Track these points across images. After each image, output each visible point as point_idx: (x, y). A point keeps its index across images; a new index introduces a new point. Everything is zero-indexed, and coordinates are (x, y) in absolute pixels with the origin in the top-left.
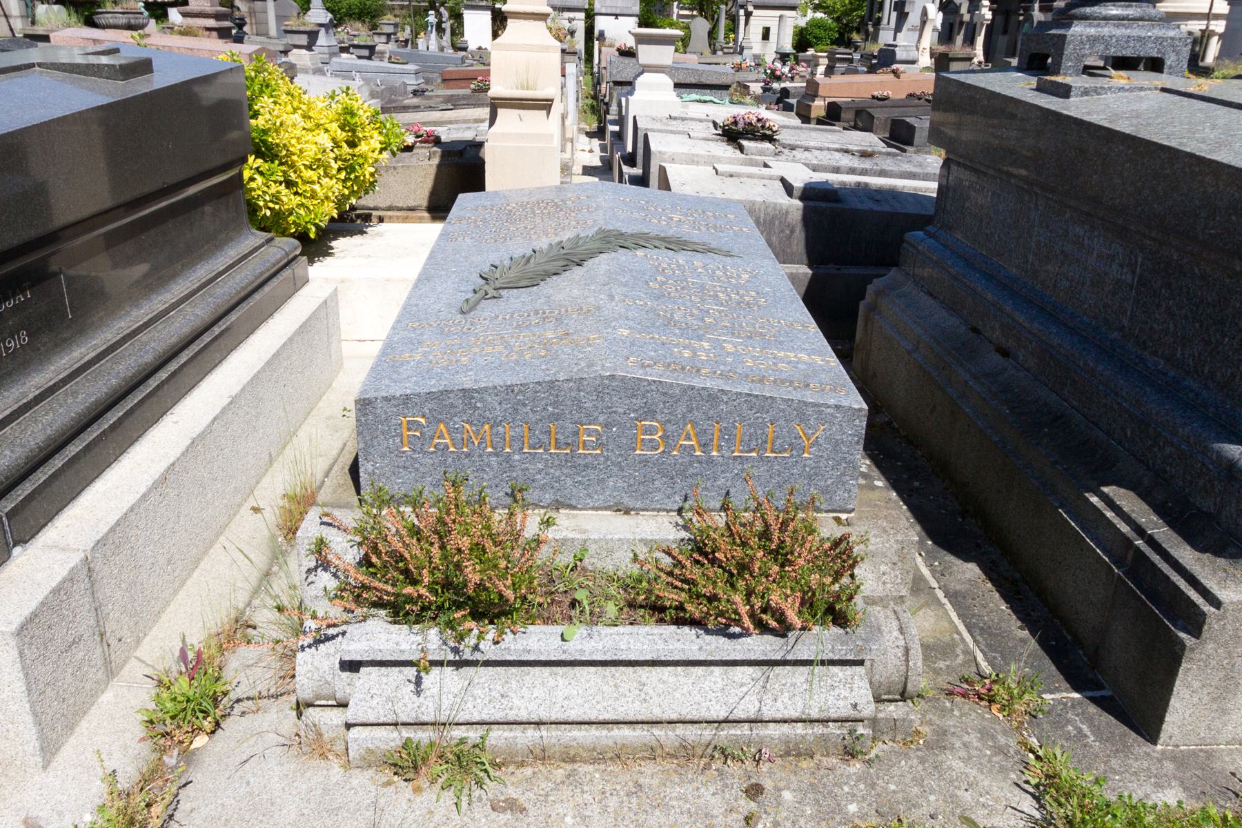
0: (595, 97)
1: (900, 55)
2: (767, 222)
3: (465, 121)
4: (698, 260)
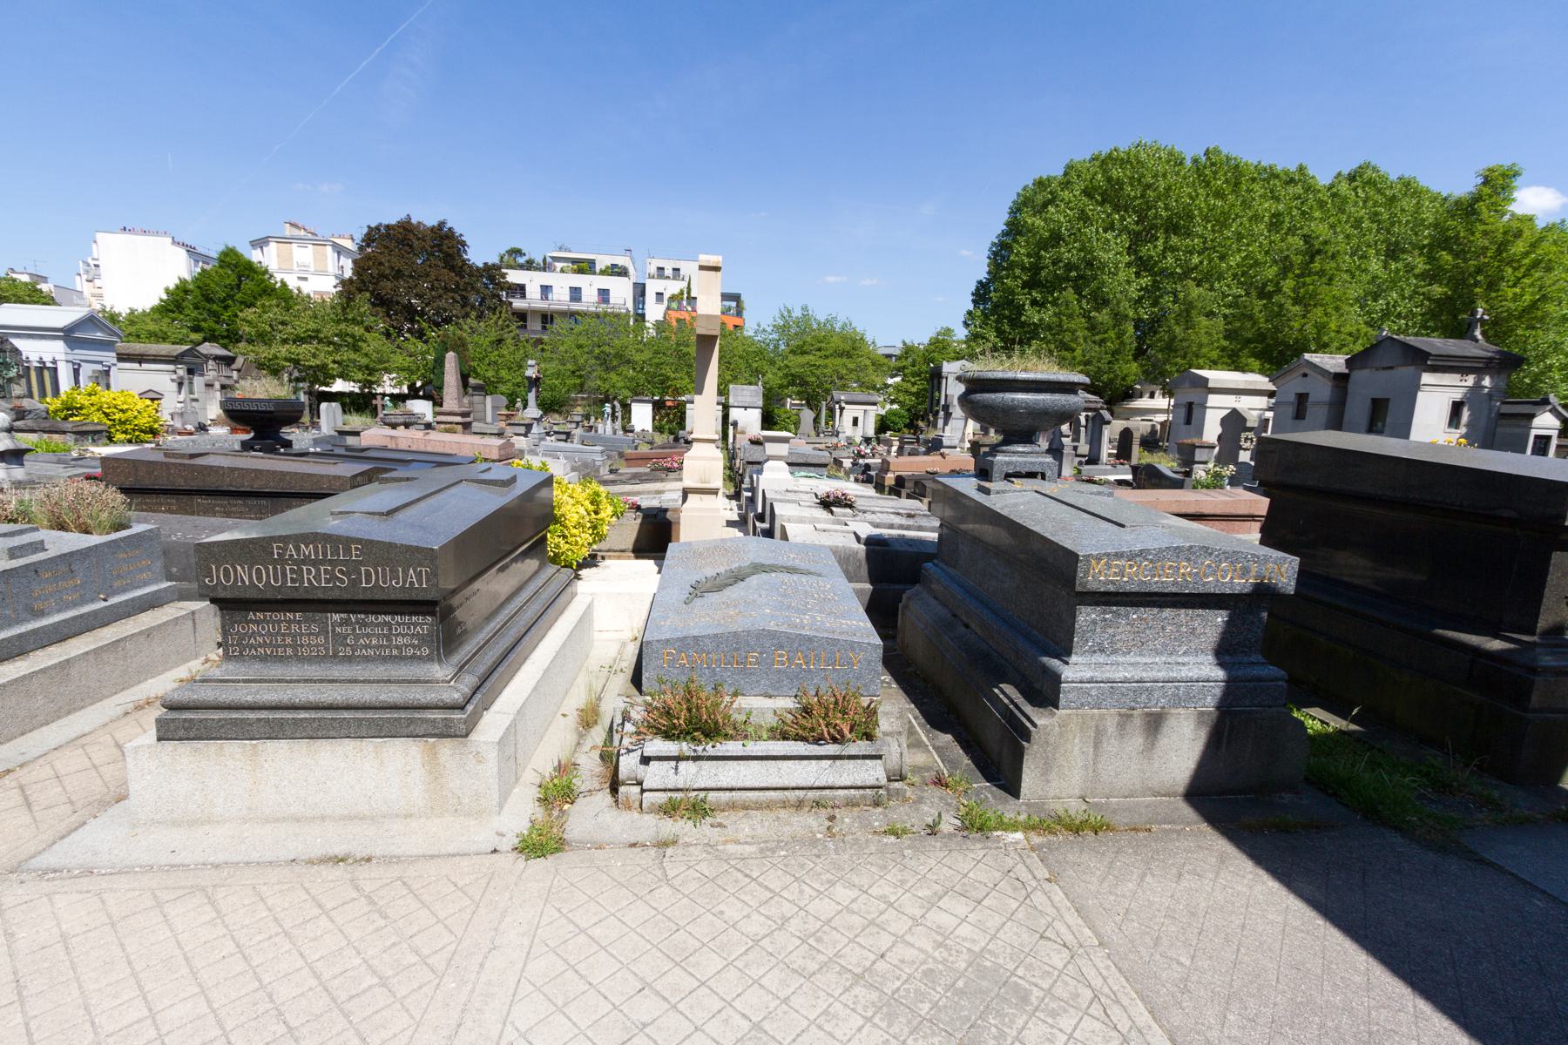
0: (731, 468)
1: (946, 442)
2: (843, 558)
3: (649, 492)
4: (804, 579)
